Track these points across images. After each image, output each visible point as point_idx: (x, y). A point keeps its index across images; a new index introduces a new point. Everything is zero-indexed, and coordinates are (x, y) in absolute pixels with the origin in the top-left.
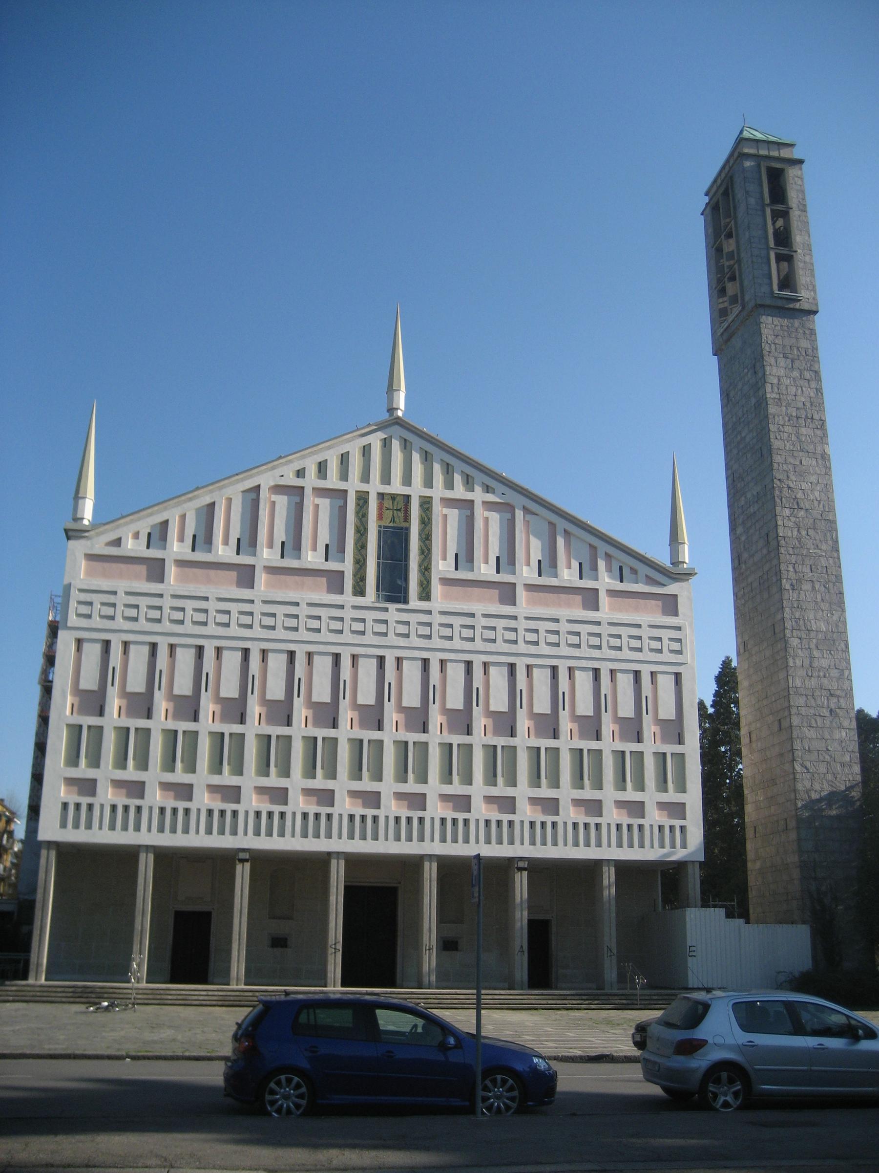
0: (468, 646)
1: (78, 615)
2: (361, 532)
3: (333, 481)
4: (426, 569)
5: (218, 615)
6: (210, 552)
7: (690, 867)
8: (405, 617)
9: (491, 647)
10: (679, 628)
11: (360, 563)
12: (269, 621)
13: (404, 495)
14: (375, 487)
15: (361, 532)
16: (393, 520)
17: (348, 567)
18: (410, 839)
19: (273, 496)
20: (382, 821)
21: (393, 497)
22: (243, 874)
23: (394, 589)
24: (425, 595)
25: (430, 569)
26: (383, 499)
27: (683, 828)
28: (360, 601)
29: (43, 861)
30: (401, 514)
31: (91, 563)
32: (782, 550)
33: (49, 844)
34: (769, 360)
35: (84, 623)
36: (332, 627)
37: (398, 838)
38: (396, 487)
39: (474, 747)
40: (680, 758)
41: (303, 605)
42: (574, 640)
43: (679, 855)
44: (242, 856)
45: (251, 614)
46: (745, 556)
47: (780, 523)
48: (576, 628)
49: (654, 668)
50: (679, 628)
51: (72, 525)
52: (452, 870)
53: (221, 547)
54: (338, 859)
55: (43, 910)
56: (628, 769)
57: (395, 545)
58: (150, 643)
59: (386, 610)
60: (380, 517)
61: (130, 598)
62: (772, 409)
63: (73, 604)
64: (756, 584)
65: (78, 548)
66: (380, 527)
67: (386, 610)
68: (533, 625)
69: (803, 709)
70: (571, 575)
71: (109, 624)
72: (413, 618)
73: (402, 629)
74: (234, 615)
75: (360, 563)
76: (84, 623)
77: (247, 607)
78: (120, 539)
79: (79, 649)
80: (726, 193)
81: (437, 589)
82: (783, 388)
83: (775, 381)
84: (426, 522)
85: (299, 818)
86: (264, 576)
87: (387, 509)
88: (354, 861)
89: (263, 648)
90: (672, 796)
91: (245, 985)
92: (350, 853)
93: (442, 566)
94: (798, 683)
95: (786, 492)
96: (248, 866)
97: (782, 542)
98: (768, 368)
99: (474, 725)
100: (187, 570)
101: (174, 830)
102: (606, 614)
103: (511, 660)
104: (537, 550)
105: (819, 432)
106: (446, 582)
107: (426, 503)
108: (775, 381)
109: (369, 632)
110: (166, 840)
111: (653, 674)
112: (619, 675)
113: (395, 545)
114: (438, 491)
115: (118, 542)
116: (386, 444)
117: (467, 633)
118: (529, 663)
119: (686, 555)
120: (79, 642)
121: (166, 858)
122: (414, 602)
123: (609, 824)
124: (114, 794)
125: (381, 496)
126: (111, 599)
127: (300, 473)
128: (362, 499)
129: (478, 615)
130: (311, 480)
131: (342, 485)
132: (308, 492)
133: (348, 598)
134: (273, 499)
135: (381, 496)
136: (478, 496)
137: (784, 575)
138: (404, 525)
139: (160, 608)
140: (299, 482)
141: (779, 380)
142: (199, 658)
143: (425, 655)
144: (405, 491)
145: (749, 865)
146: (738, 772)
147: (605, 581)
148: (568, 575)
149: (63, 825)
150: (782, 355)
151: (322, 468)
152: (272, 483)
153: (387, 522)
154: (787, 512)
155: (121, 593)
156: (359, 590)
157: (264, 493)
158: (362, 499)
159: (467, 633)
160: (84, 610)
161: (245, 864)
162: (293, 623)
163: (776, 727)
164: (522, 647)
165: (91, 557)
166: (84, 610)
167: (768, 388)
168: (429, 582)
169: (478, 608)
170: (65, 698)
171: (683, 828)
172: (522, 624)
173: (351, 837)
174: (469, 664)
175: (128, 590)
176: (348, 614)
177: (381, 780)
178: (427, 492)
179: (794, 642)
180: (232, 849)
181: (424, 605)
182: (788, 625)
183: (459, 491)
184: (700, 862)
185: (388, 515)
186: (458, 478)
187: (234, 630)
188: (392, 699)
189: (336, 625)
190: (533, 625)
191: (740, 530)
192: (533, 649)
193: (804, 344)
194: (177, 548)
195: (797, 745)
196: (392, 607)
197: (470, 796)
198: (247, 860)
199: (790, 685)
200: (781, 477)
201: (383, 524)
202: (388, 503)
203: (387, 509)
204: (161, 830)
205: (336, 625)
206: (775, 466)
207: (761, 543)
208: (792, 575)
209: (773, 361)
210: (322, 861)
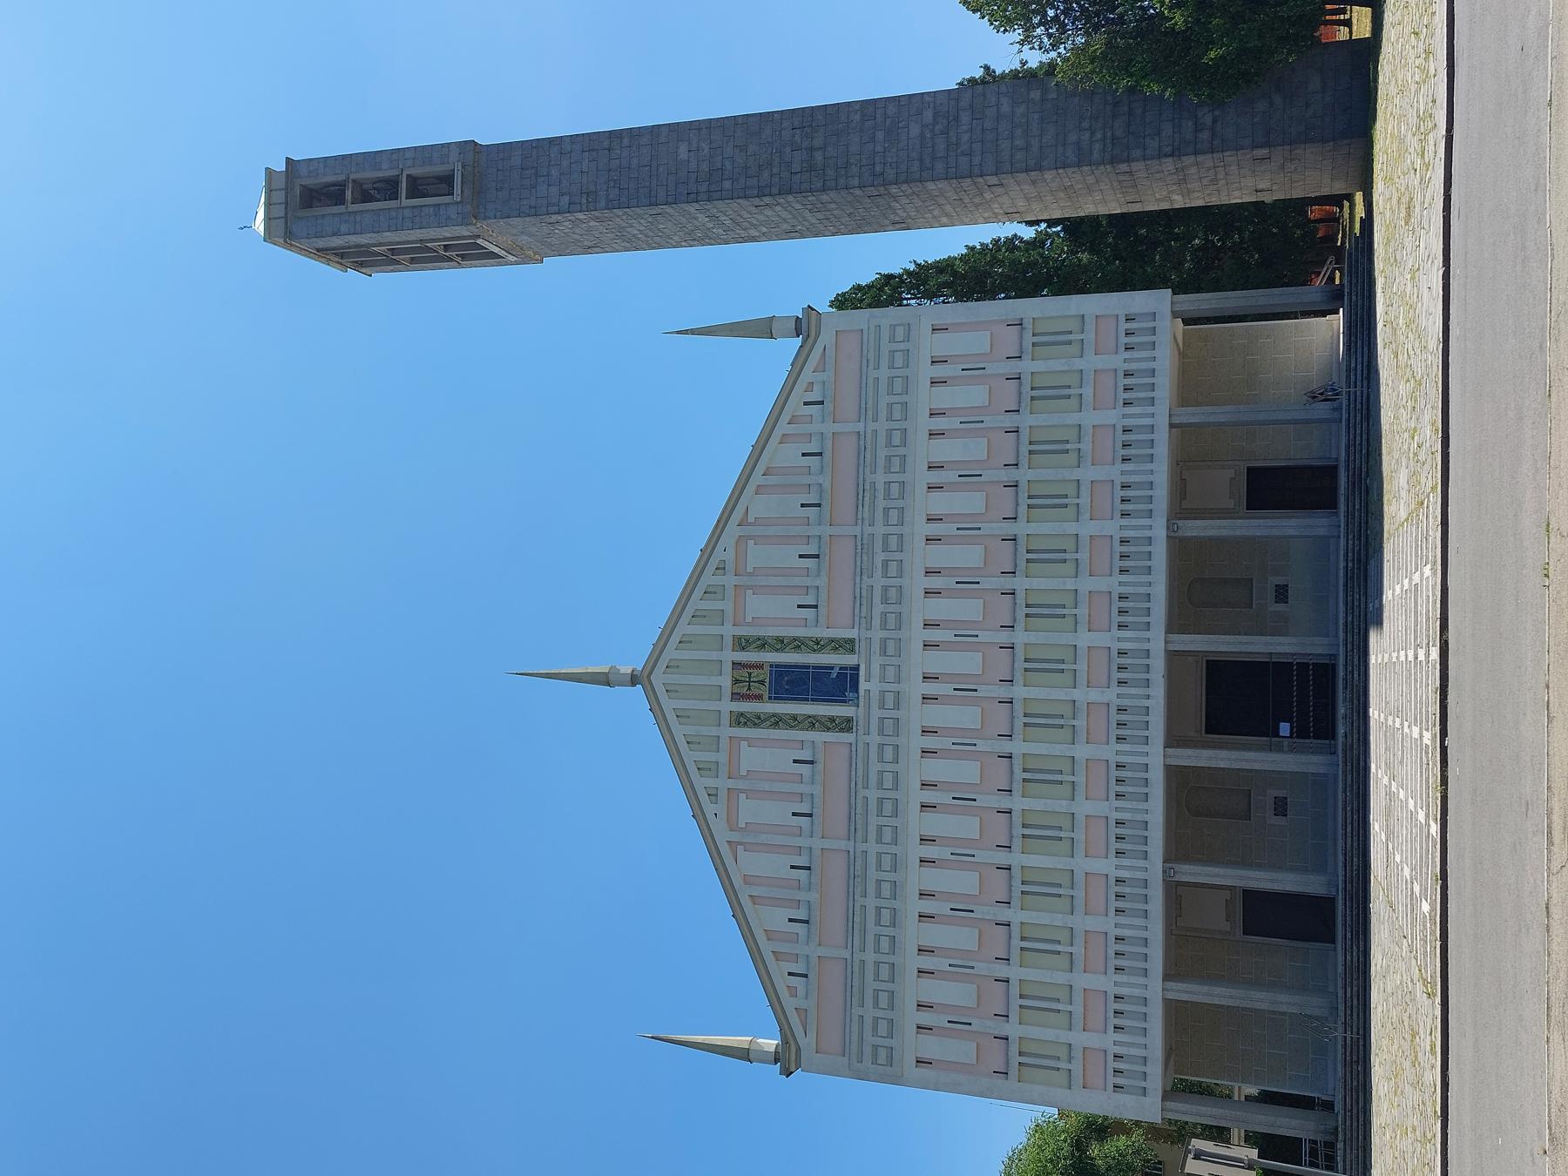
7: (1170, 996)
16: (762, 682)
20: (1123, 590)
22: (1190, 873)
23: (842, 685)
24: (848, 645)
30: (755, 672)
46: (785, 226)
57: (793, 683)
60: (759, 698)
64: (820, 216)
80: (342, 256)
88: (1174, 739)
105: (626, 141)
107: (742, 643)
113: (793, 683)
127: (713, 795)
138: (767, 669)
145: (1177, 206)
146: (1054, 46)
163: (1000, 190)
191: (754, 233)
193: (517, 160)
201: (766, 696)
207: (769, 212)
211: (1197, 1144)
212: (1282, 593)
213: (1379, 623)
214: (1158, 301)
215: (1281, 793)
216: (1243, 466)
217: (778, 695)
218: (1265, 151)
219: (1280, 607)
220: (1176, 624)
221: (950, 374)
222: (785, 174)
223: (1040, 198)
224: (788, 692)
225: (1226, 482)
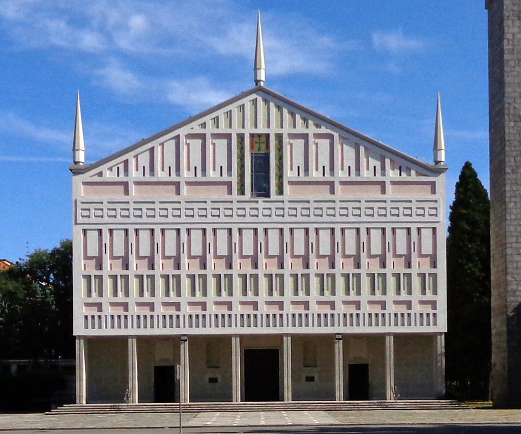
0: (306, 219)
1: (83, 216)
2: (241, 158)
3: (223, 129)
4: (280, 177)
5: (200, 211)
6: (154, 176)
8: (268, 205)
9: (319, 219)
10: (436, 201)
11: (242, 176)
12: (190, 213)
13: (266, 134)
14: (248, 130)
15: (241, 158)
16: (259, 149)
17: (234, 179)
18: (377, 325)
19: (213, 140)
20: (387, 317)
21: (259, 135)
23: (261, 189)
24: (280, 191)
25: (283, 176)
26: (253, 137)
27: (435, 315)
28: (242, 198)
29: (77, 345)
31: (189, 186)
32: (507, 149)
33: (80, 337)
34: (507, 23)
35: (86, 220)
36: (393, 213)
37: (370, 325)
38: (261, 129)
39: (310, 275)
40: (434, 276)
41: (209, 202)
42: (370, 212)
43: (431, 329)
44: (338, 337)
45: (231, 209)
47: (507, 131)
48: (371, 205)
49: (420, 225)
50: (436, 201)
51: (74, 167)
52: (301, 341)
53: (340, 172)
54: (236, 337)
55: (80, 369)
56: (403, 282)
57: (261, 165)
58: (150, 229)
59: (257, 202)
60: (252, 147)
61: (316, 204)
62: (506, 57)
63: (79, 211)
65: (78, 180)
66: (252, 154)
67: (257, 202)
68: (344, 205)
69: (515, 244)
70: (368, 174)
71: (100, 220)
72: (273, 206)
73: (267, 212)
74: (170, 211)
75: (242, 176)
76: (86, 220)
77: (177, 206)
78: (102, 172)
79: (85, 234)
81: (287, 188)
82: (516, 41)
83: (510, 37)
84: (280, 149)
85: (213, 317)
86: (391, 186)
87: (256, 143)
88: (242, 337)
89: (187, 227)
90: (429, 296)
91: (292, 401)
92: (397, 333)
93: (289, 174)
94: (512, 229)
95: (512, 111)
96: (187, 343)
97: (507, 143)
98: (506, 29)
99: (310, 263)
100: (87, 186)
101: (171, 326)
102: (390, 195)
103: (332, 226)
104: (350, 161)
106: (291, 183)
107: (279, 137)
108: (510, 37)
109: (248, 215)
110: (142, 332)
111: (393, 229)
112: (346, 231)
113: (261, 165)
114: (286, 130)
115: (100, 174)
116: (255, 102)
117: (305, 212)
118: (316, 227)
119: (442, 156)
120: (85, 231)
121: (143, 341)
122: (274, 196)
123: (390, 314)
124: (164, 310)
125: (252, 135)
126: (100, 206)
127: (204, 125)
128: (241, 137)
129: (414, 201)
130: (210, 129)
131: (228, 131)
132: (208, 137)
133: (235, 196)
134: (291, 142)
135: (252, 135)
136: (312, 130)
137: (508, 164)
139: (283, 209)
140: (202, 131)
141: (513, 36)
142: (307, 235)
143: (357, 226)
144: (266, 131)
145: (492, 331)
147: (392, 174)
148: (366, 174)
149: (86, 327)
150: (517, 18)
151: (216, 120)
152: (187, 133)
153: (256, 151)
154: (512, 124)
155: (105, 202)
156: (242, 192)
157: (183, 140)
158: (241, 137)
159: (305, 212)
160: (86, 213)
161: (185, 342)
162: (203, 213)
164: (338, 218)
165: (85, 183)
166: (86, 213)
167: (505, 42)
168: (282, 184)
169: (311, 198)
170: (80, 261)
171: (435, 315)
172: (287, 205)
173: (242, 326)
174: (307, 230)
175: (418, 199)
176: (235, 205)
177: (232, 296)
178: (280, 131)
179: (511, 205)
180: (125, 336)
181: (280, 198)
182: (508, 194)
183: (300, 128)
184: (445, 333)
185: (256, 146)
186: (311, 123)
187: (171, 219)
188: (391, 250)
189: (229, 212)
190: (344, 205)
192: (344, 219)
194: (135, 174)
195: (509, 266)
196: (260, 200)
197: (309, 302)
198: (186, 340)
199: (507, 230)
200: (509, 102)
202: (256, 139)
203: (256, 143)
204: (139, 327)
205: (229, 212)
206: (506, 94)
208: (513, 164)
209: (510, 22)
210: (227, 339)
211: (491, 406)
212: (310, 379)
213: (457, 183)
214: (442, 325)
215: (219, 380)
216: (370, 362)
217: (254, 158)
218: (507, 369)
219: (304, 378)
220: (295, 338)
221: (360, 318)
222: (515, 153)
223: (498, 272)
224: (255, 162)
225: (362, 355)
